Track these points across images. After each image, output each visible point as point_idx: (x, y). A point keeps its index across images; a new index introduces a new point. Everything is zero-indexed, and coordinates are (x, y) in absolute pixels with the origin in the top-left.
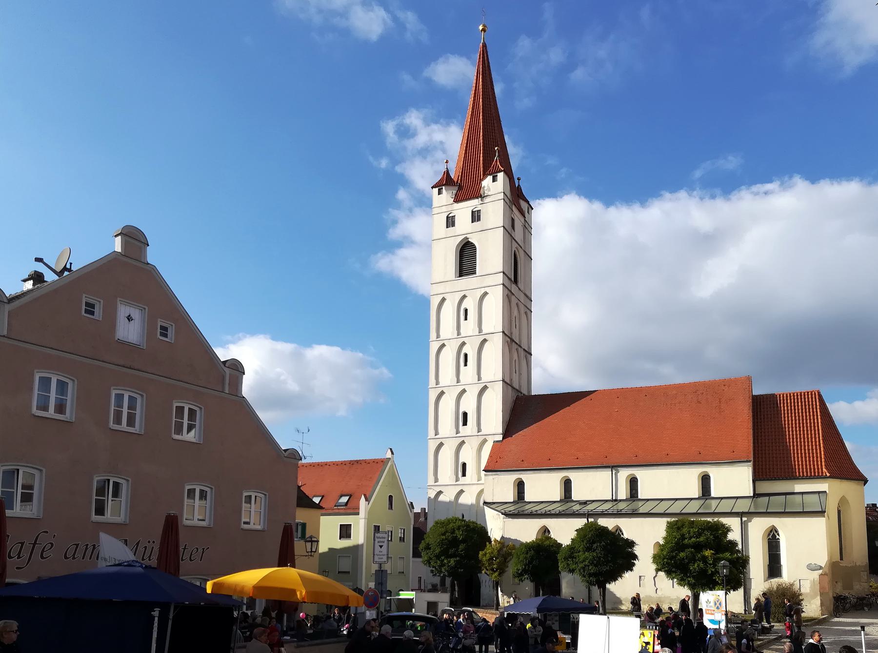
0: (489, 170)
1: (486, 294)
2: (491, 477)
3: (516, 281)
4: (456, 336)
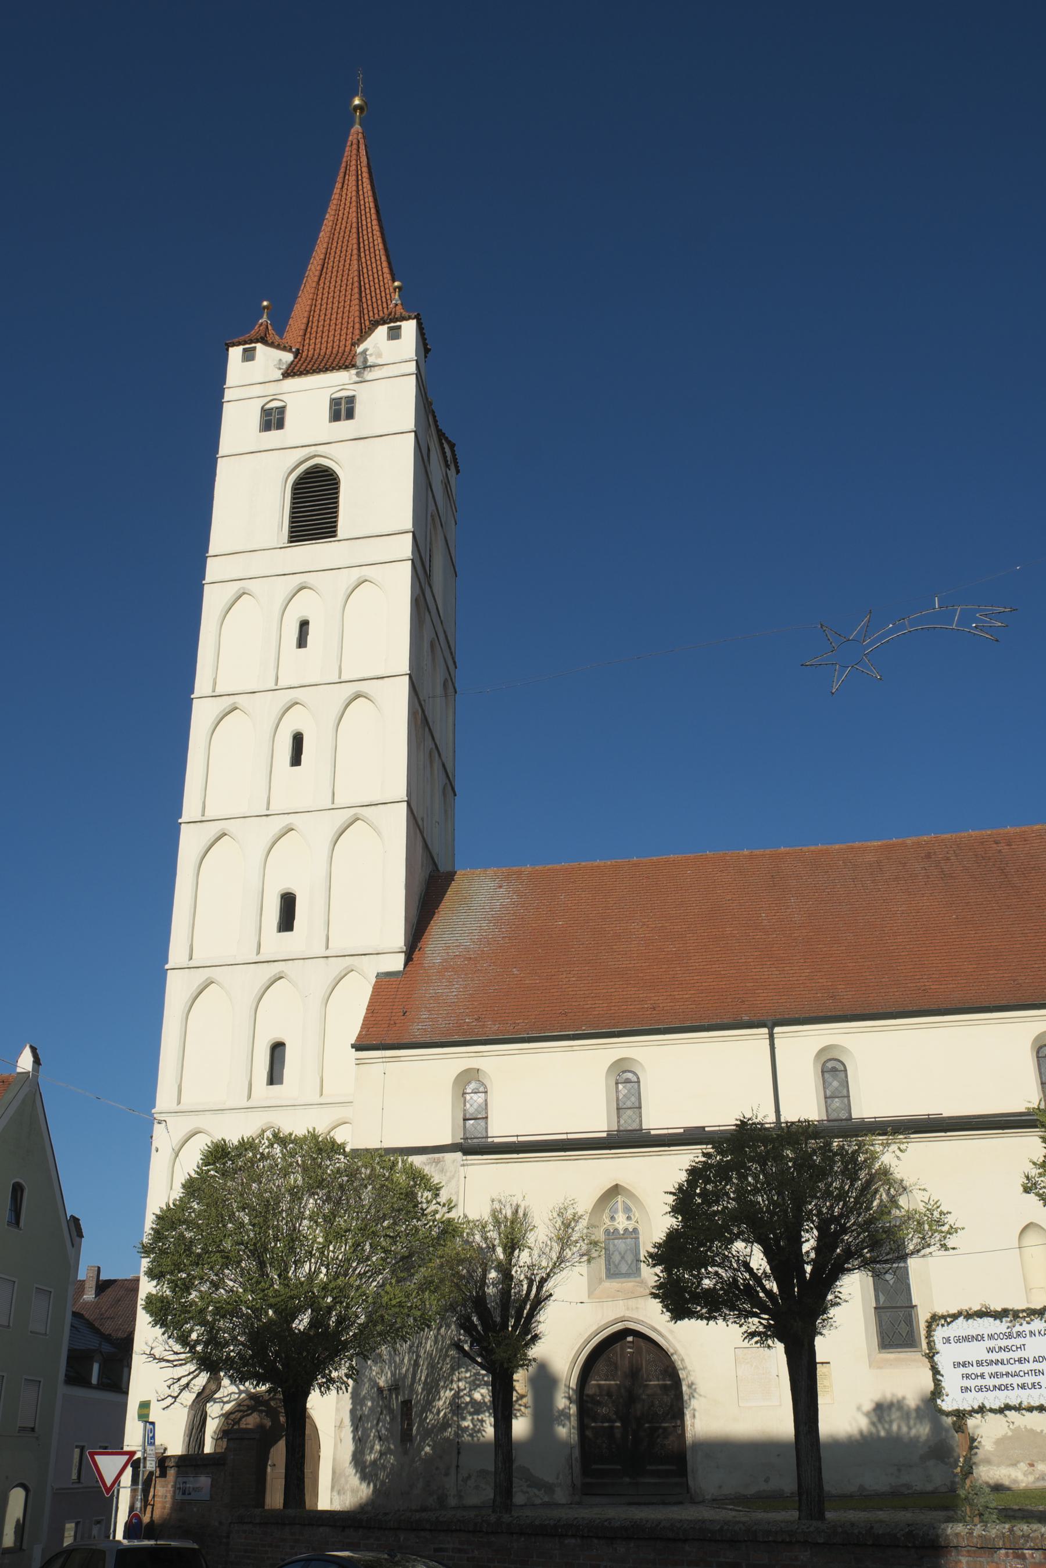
2: (377, 1069)
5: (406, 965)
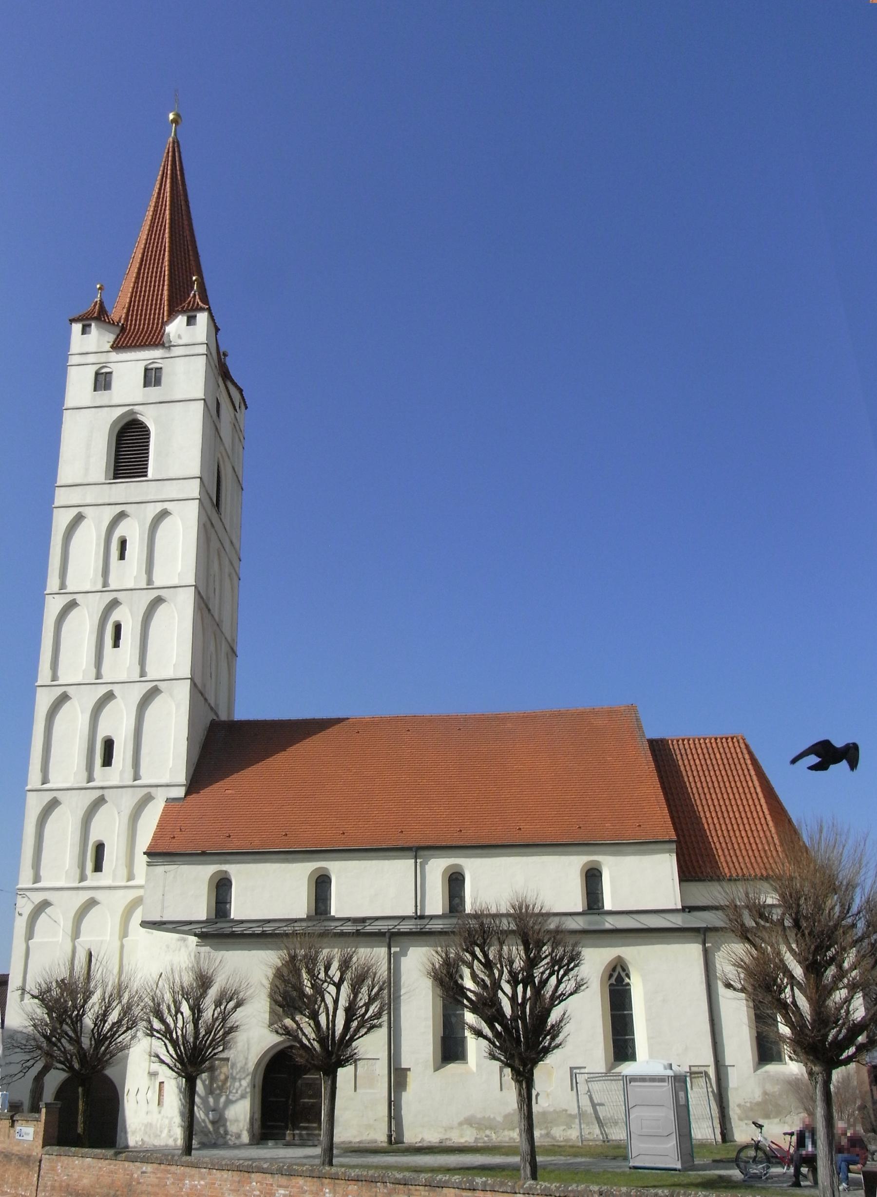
0: (181, 303)
1: (45, 904)
2: (160, 869)
3: (218, 505)
4: (99, 587)
5: (185, 796)
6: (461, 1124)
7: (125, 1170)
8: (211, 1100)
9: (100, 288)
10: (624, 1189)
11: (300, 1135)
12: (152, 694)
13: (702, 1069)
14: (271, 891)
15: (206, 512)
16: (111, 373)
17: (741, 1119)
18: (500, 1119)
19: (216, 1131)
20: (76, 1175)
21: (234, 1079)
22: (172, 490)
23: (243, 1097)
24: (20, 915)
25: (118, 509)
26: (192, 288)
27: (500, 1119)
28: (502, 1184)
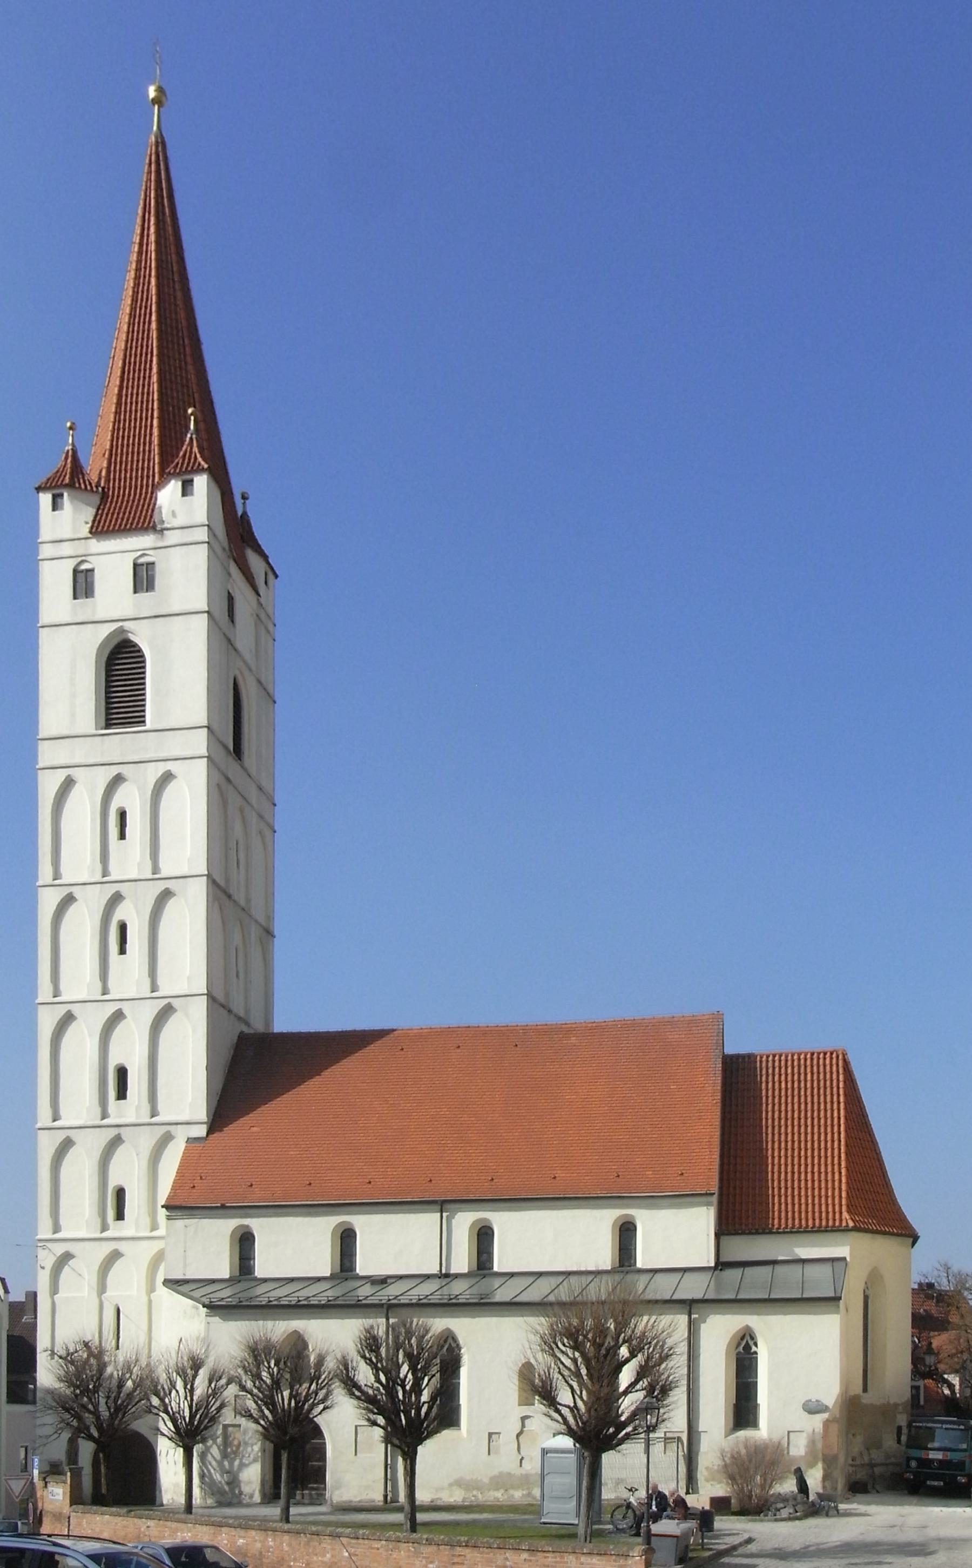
0: (173, 464)
2: (180, 1224)
4: (98, 877)
6: (451, 1485)
7: (135, 1524)
8: (226, 1463)
9: (71, 428)
10: (442, 1537)
11: (310, 1495)
12: (166, 1012)
13: (676, 1435)
14: (294, 1248)
15: (219, 769)
16: (92, 570)
17: (707, 1480)
18: (486, 1480)
19: (232, 1490)
20: (97, 1530)
21: (246, 1444)
22: (176, 745)
23: (255, 1460)
24: (43, 1268)
25: (114, 771)
26: (188, 428)
27: (486, 1480)
28: (374, 1534)
